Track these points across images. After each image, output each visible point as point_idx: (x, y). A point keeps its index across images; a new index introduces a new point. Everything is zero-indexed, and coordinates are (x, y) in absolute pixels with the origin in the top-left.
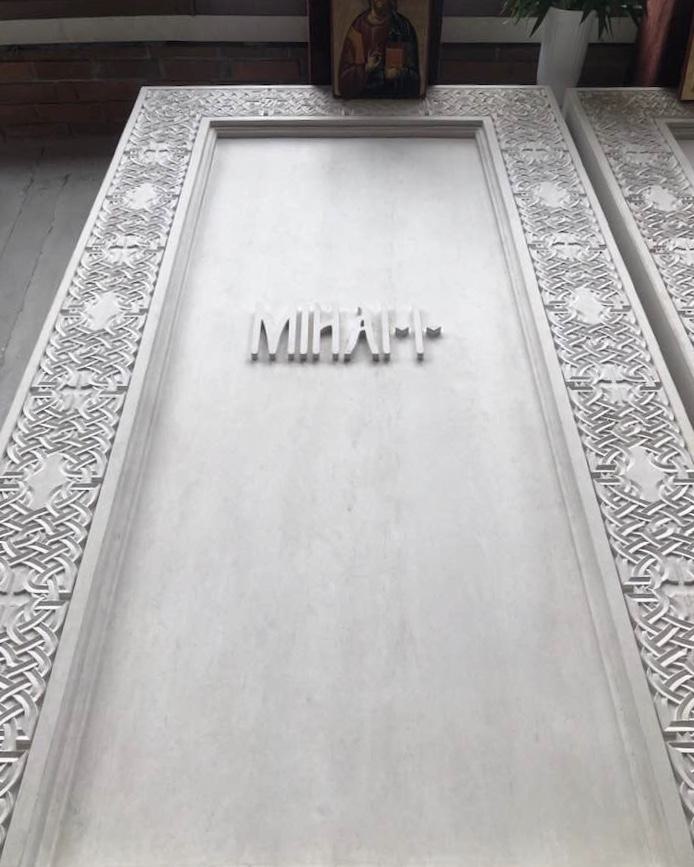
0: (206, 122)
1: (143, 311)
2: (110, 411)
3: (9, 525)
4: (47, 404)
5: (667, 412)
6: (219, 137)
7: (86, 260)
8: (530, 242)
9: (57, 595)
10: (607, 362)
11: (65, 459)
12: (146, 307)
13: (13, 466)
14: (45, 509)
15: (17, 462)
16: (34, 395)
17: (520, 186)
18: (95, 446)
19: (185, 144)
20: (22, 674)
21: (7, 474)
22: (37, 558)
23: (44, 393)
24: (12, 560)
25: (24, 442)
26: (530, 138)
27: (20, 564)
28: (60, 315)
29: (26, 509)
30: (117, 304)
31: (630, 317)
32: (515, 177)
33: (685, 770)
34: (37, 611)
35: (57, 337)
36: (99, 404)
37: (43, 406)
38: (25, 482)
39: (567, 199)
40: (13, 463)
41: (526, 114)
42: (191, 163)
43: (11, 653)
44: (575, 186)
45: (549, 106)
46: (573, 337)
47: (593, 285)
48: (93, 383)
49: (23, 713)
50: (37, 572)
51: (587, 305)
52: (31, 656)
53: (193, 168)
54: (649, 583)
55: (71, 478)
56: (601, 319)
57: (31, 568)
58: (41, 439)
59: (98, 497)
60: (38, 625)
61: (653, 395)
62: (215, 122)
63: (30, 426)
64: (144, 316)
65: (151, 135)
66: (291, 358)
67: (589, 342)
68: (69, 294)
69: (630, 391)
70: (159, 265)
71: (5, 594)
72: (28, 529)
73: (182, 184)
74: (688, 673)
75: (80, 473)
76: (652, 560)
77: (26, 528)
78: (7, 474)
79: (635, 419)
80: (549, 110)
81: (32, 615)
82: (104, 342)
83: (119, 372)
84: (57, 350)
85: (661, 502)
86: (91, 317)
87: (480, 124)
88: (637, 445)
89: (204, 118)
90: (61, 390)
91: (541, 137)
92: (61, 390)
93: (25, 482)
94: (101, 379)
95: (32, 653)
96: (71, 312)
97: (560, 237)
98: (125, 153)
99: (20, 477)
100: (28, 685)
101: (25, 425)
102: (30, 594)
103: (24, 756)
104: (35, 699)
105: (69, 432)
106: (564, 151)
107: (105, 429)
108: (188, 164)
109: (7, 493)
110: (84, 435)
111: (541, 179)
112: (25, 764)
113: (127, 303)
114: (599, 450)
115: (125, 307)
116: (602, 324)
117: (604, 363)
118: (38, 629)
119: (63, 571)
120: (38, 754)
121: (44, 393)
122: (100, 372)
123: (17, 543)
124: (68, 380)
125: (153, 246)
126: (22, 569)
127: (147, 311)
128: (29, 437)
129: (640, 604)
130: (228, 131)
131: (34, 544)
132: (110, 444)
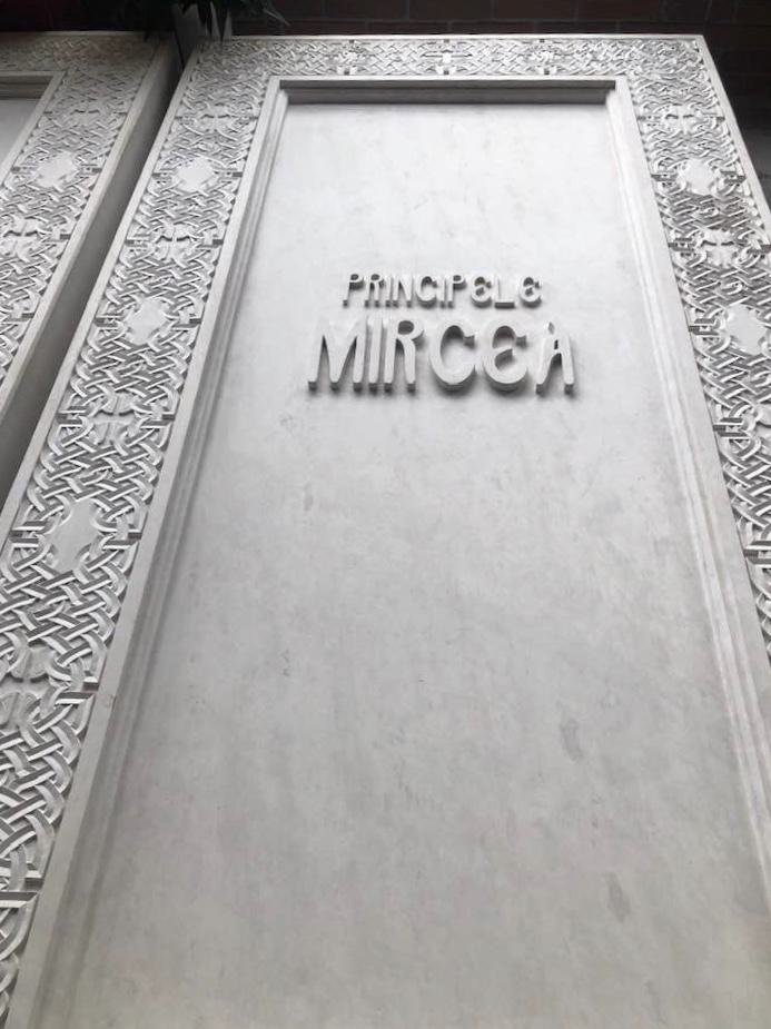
0: (275, 82)
6: (292, 103)
7: (126, 257)
8: (655, 172)
13: (79, 400)
15: (84, 395)
16: (98, 326)
18: (137, 473)
23: (75, 422)
25: (54, 466)
27: (124, 390)
28: (94, 326)
29: (51, 571)
31: (744, 188)
32: (655, 153)
33: (764, 583)
35: (90, 351)
38: (125, 323)
39: (721, 184)
40: (78, 395)
41: (672, 71)
42: (257, 131)
43: (77, 593)
45: (702, 62)
49: (34, 838)
51: (698, 177)
52: (103, 572)
54: (741, 424)
57: (134, 394)
58: (108, 372)
59: (133, 563)
60: (105, 564)
62: (285, 81)
64: (196, 329)
66: (358, 389)
68: (104, 296)
69: (735, 255)
72: (132, 361)
73: (245, 158)
74: (765, 464)
77: (159, 274)
80: (702, 67)
82: (147, 359)
83: (216, 227)
84: (91, 368)
90: (95, 416)
92: (157, 242)
93: (125, 323)
94: (109, 520)
95: (85, 636)
96: (106, 321)
97: (672, 110)
98: (177, 118)
100: (51, 773)
101: (90, 357)
105: (137, 365)
106: (718, 119)
107: (202, 277)
108: (253, 132)
109: (72, 428)
110: (121, 475)
112: (36, 906)
113: (109, 520)
114: (726, 401)
117: (762, 403)
118: (105, 568)
119: (132, 510)
121: (75, 422)
125: (208, 239)
128: (62, 460)
130: (306, 95)
131: (101, 482)
132: (182, 379)
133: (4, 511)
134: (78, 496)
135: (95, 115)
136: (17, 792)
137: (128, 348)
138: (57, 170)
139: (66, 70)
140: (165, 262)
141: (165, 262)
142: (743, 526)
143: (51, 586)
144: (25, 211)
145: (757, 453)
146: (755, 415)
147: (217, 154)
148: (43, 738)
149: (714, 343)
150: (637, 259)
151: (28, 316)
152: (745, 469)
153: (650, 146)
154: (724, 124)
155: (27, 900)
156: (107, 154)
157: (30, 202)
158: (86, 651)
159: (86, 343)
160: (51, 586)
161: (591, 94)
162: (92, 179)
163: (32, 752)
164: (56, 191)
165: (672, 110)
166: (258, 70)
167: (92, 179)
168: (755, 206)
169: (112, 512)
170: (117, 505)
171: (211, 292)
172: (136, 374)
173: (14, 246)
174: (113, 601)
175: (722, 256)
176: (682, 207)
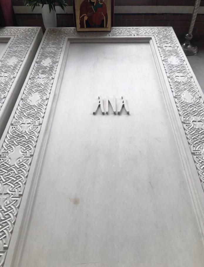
0: (67, 38)
1: (47, 99)
2: (36, 132)
3: (3, 170)
4: (17, 129)
5: (194, 83)
6: (71, 43)
7: (11, 130)
8: (168, 76)
9: (2, 248)
10: (195, 115)
11: (22, 148)
12: (48, 98)
13: (16, 120)
14: (14, 165)
15: (6, 149)
17: (159, 44)
18: (31, 143)
19: (60, 45)
20: (6, 222)
21: (3, 153)
22: (23, 145)
24: (4, 182)
26: (167, 43)
27: (6, 184)
30: (38, 96)
31: (185, 63)
33: (201, 171)
34: (12, 200)
36: (10, 203)
37: (25, 103)
41: (165, 35)
44: (175, 44)
45: (172, 33)
46: (184, 107)
47: (189, 91)
48: (31, 122)
49: (6, 237)
50: (12, 187)
51: (174, 60)
53: (54, 86)
54: (189, 121)
55: (23, 155)
56: (192, 101)
57: (10, 185)
59: (47, 104)
61: (199, 100)
62: (70, 38)
63: (20, 113)
65: (50, 42)
67: (173, 69)
68: (24, 93)
70: (52, 84)
71: (1, 194)
75: (35, 122)
76: (200, 146)
78: (3, 153)
79: (194, 107)
80: (172, 34)
81: (10, 201)
82: (26, 137)
83: (39, 119)
85: (192, 103)
86: (30, 101)
87: (151, 38)
88: (186, 91)
89: (66, 37)
90: (21, 124)
91: (170, 42)
92: (21, 124)
95: (19, 182)
96: (14, 125)
97: (177, 74)
99: (18, 123)
102: (9, 194)
103: (6, 253)
104: (10, 231)
106: (177, 47)
111: (171, 55)
113: (42, 96)
115: (41, 97)
116: (192, 103)
117: (194, 116)
119: (20, 187)
120: (25, 197)
122: (42, 94)
123: (5, 176)
124: (23, 121)
126: (7, 186)
127: (48, 99)
129: (197, 157)
132: (44, 114)
133: (1, 140)
134: (17, 145)
135: (22, 47)
136: (15, 177)
137: (9, 166)
138: (12, 61)
139: (15, 36)
140: (39, 84)
141: (39, 84)
142: (191, 146)
143: (9, 169)
144: (4, 71)
145: (192, 128)
146: (192, 119)
147: (52, 57)
148: (6, 216)
149: (180, 100)
150: (186, 179)
151: (5, 98)
152: (190, 132)
153: (160, 51)
154: (178, 48)
155: (4, 253)
156: (31, 44)
157: (5, 69)
158: (19, 186)
159: (19, 105)
160: (9, 169)
161: (146, 41)
162: (21, 63)
163: (5, 212)
164: (12, 66)
165: (166, 45)
166: (63, 35)
167: (21, 63)
168: (189, 70)
169: (34, 120)
170: (27, 148)
171: (40, 134)
172: (23, 141)
173: (1, 80)
174: (25, 178)
175: (180, 79)
176: (178, 87)
